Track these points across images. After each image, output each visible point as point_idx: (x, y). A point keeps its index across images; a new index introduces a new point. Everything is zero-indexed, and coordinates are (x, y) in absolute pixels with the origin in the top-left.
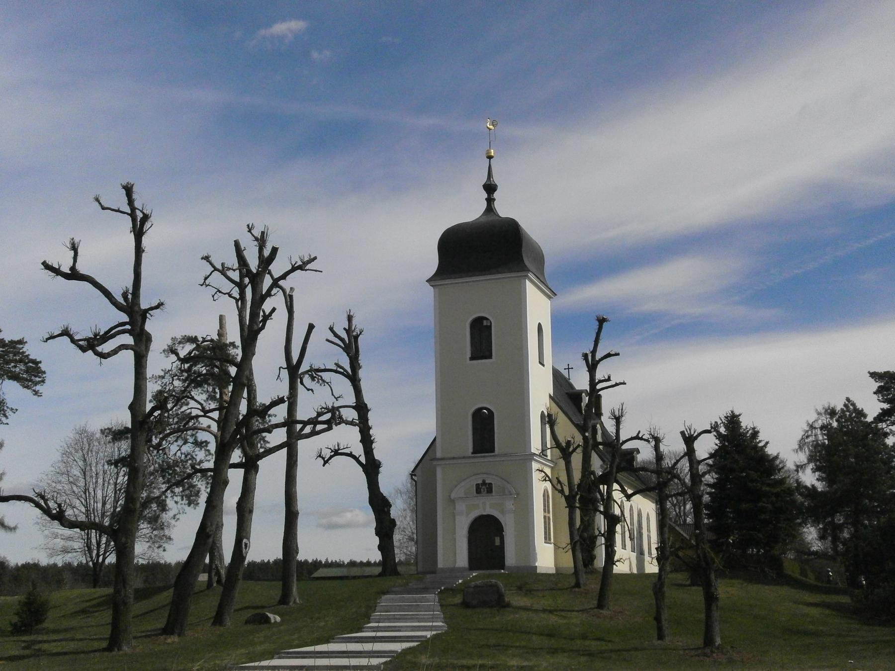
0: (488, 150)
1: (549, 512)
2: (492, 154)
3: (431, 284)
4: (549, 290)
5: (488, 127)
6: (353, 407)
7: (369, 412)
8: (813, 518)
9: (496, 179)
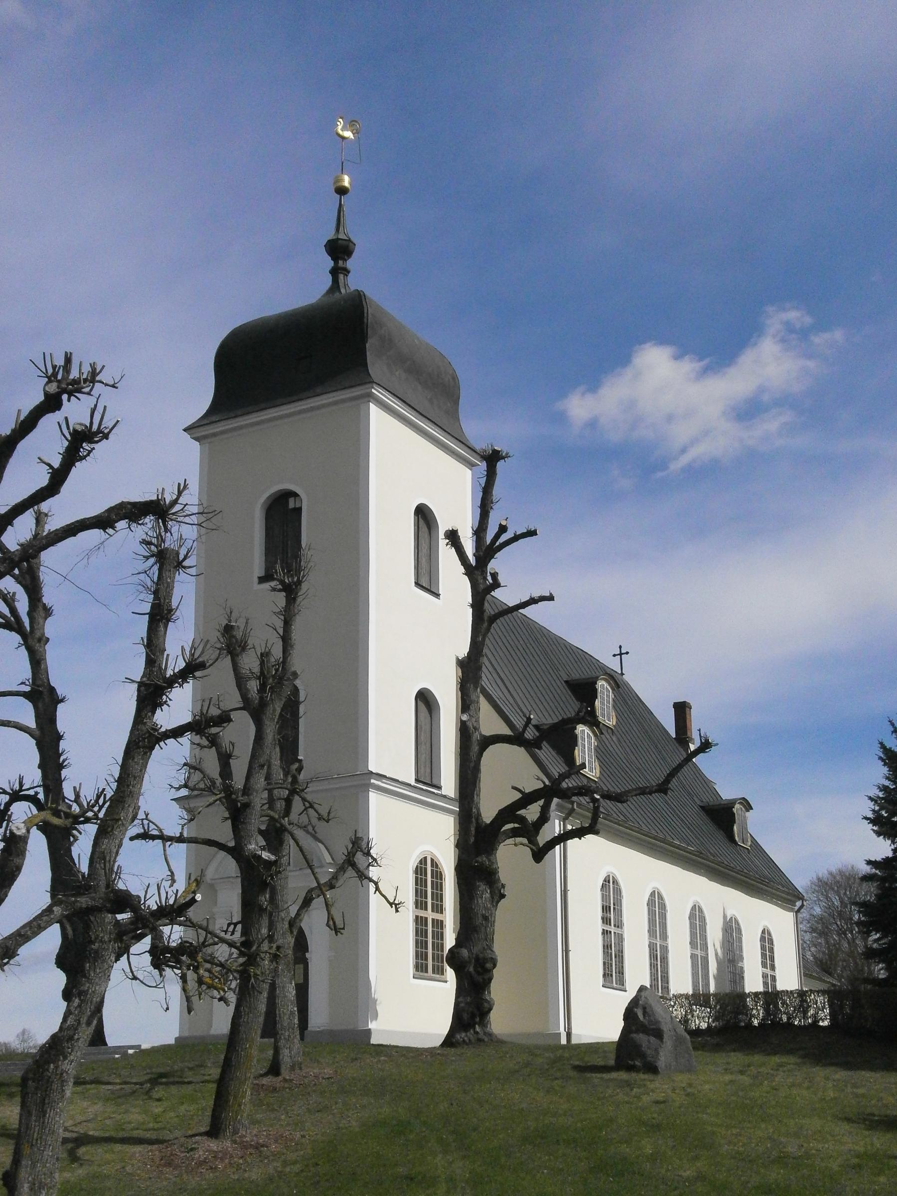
1: (439, 908)
3: (194, 436)
4: (466, 448)
6: (25, 695)
7: (60, 707)
8: (468, 763)
9: (353, 231)
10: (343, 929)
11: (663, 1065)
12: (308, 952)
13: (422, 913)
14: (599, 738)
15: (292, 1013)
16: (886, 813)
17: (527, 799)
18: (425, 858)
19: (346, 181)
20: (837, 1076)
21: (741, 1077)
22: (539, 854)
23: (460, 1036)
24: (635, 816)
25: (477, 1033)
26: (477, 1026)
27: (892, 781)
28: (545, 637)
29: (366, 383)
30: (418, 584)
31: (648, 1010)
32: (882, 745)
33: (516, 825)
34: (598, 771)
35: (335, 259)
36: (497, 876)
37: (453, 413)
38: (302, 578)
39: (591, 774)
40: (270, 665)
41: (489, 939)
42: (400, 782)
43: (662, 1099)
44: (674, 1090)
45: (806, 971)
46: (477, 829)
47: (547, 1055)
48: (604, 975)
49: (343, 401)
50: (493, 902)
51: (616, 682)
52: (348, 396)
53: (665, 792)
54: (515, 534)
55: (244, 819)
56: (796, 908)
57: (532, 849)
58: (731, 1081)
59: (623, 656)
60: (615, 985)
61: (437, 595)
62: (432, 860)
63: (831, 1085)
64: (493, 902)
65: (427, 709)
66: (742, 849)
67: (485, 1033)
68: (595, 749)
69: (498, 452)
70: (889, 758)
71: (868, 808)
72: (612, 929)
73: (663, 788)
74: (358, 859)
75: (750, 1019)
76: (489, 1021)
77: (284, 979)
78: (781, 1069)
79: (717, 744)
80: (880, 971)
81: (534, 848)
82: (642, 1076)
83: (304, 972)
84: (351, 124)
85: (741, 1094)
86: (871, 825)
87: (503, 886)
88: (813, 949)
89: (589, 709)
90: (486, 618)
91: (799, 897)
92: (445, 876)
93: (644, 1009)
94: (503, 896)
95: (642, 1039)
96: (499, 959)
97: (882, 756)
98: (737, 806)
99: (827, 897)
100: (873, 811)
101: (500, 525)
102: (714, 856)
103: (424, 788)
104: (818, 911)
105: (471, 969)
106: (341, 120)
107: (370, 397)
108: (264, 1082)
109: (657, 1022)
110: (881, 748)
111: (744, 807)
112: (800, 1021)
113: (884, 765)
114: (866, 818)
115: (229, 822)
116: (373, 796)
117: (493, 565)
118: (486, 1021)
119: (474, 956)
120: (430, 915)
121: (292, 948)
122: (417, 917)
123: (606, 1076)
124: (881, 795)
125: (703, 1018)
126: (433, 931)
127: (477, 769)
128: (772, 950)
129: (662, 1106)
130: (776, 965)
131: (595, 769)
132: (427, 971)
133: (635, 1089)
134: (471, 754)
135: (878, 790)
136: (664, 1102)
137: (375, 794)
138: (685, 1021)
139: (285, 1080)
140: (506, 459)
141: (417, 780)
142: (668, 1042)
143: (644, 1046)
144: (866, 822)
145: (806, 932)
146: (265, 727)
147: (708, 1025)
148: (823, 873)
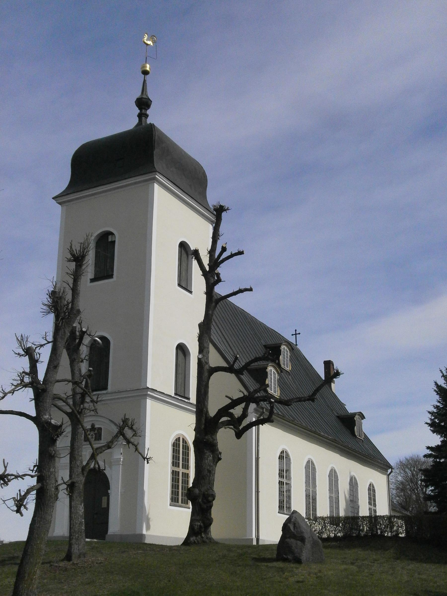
0: (144, 64)
2: (148, 69)
3: (58, 202)
5: (145, 43)
10: (105, 470)
11: (305, 559)
12: (110, 489)
13: (176, 469)
14: (280, 374)
15: (81, 523)
16: (438, 420)
17: (235, 403)
18: (179, 438)
19: (148, 68)
20: (410, 567)
21: (351, 566)
22: (239, 435)
23: (192, 539)
24: (299, 418)
25: (202, 537)
26: (203, 534)
27: (441, 403)
28: (254, 322)
29: (152, 172)
30: (179, 285)
31: (296, 525)
32: (436, 384)
33: (229, 419)
34: (279, 393)
35: (140, 109)
36: (217, 447)
37: (203, 194)
38: (86, 253)
39: (275, 394)
40: (62, 305)
41: (211, 484)
42: (165, 394)
43: (301, 580)
44: (309, 574)
45: (392, 506)
46: (206, 420)
47: (238, 551)
48: (279, 507)
49: (139, 182)
50: (214, 462)
51: (292, 348)
52: (142, 179)
53: (313, 400)
54: (231, 253)
55: (43, 399)
56: (388, 473)
57: (235, 431)
58: (345, 569)
59: (297, 335)
60: (285, 512)
61: (191, 292)
62: (183, 439)
63: (405, 572)
64: (214, 462)
65: (183, 354)
66: (359, 439)
67: (207, 538)
68: (278, 381)
69: (223, 206)
70: (440, 390)
71: (427, 418)
72: (285, 481)
73: (311, 398)
74: (126, 431)
75: (359, 532)
76: (210, 531)
77: (77, 502)
78: (376, 562)
79: (343, 373)
80: (433, 508)
81: (236, 430)
82: (292, 565)
83: (107, 499)
84: (151, 37)
85: (350, 577)
86: (429, 427)
87: (220, 453)
88: (398, 498)
89: (270, 352)
90: (214, 300)
91: (390, 467)
92: (190, 448)
93: (294, 524)
94: (220, 459)
95: (292, 542)
96: (217, 495)
97: (436, 389)
98: (357, 416)
99: (405, 471)
100: (431, 419)
101: (222, 247)
102: (343, 442)
103: (180, 398)
104: (400, 478)
105: (200, 500)
106: (146, 35)
107: (155, 179)
108: (60, 565)
109: (302, 532)
110: (435, 385)
111: (360, 416)
112: (388, 534)
113: (437, 394)
114: (427, 423)
115: (34, 401)
116: (149, 402)
117: (219, 270)
118: (208, 531)
119: (202, 493)
120: (181, 470)
121: (83, 484)
122: (173, 471)
123: (270, 564)
124: (435, 410)
125: (332, 531)
126: (182, 480)
127: (207, 386)
128: (374, 496)
129: (300, 584)
130: (377, 504)
131: (277, 392)
132: (178, 502)
133: (286, 573)
134: (204, 377)
135: (434, 408)
136: (302, 582)
137: (150, 400)
138: (321, 533)
139: (74, 564)
140: (227, 211)
141: (176, 394)
142: (308, 545)
143: (293, 547)
144: (427, 425)
145: (393, 489)
146: (58, 343)
147: (334, 535)
148: (403, 459)
